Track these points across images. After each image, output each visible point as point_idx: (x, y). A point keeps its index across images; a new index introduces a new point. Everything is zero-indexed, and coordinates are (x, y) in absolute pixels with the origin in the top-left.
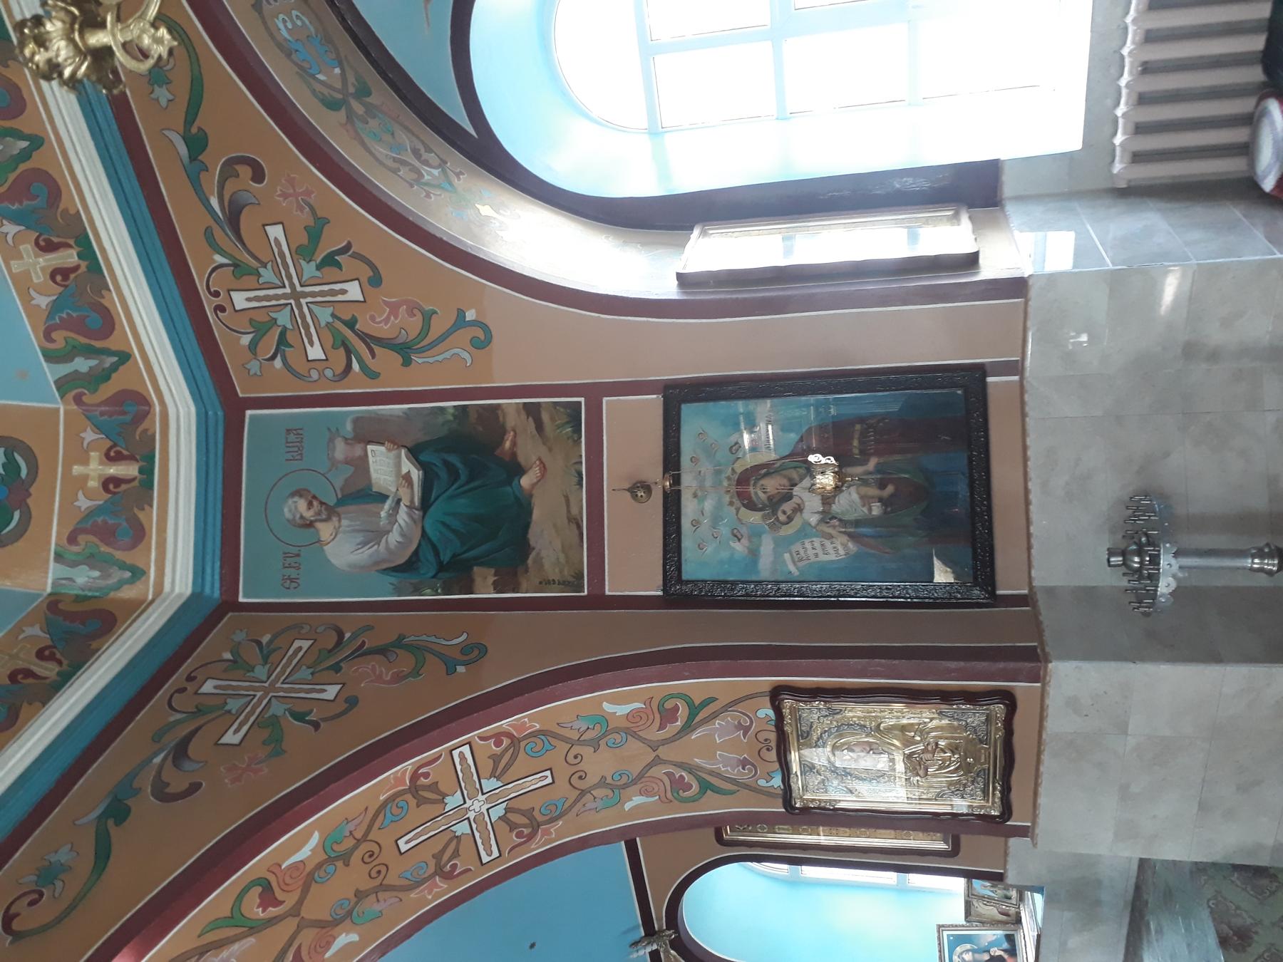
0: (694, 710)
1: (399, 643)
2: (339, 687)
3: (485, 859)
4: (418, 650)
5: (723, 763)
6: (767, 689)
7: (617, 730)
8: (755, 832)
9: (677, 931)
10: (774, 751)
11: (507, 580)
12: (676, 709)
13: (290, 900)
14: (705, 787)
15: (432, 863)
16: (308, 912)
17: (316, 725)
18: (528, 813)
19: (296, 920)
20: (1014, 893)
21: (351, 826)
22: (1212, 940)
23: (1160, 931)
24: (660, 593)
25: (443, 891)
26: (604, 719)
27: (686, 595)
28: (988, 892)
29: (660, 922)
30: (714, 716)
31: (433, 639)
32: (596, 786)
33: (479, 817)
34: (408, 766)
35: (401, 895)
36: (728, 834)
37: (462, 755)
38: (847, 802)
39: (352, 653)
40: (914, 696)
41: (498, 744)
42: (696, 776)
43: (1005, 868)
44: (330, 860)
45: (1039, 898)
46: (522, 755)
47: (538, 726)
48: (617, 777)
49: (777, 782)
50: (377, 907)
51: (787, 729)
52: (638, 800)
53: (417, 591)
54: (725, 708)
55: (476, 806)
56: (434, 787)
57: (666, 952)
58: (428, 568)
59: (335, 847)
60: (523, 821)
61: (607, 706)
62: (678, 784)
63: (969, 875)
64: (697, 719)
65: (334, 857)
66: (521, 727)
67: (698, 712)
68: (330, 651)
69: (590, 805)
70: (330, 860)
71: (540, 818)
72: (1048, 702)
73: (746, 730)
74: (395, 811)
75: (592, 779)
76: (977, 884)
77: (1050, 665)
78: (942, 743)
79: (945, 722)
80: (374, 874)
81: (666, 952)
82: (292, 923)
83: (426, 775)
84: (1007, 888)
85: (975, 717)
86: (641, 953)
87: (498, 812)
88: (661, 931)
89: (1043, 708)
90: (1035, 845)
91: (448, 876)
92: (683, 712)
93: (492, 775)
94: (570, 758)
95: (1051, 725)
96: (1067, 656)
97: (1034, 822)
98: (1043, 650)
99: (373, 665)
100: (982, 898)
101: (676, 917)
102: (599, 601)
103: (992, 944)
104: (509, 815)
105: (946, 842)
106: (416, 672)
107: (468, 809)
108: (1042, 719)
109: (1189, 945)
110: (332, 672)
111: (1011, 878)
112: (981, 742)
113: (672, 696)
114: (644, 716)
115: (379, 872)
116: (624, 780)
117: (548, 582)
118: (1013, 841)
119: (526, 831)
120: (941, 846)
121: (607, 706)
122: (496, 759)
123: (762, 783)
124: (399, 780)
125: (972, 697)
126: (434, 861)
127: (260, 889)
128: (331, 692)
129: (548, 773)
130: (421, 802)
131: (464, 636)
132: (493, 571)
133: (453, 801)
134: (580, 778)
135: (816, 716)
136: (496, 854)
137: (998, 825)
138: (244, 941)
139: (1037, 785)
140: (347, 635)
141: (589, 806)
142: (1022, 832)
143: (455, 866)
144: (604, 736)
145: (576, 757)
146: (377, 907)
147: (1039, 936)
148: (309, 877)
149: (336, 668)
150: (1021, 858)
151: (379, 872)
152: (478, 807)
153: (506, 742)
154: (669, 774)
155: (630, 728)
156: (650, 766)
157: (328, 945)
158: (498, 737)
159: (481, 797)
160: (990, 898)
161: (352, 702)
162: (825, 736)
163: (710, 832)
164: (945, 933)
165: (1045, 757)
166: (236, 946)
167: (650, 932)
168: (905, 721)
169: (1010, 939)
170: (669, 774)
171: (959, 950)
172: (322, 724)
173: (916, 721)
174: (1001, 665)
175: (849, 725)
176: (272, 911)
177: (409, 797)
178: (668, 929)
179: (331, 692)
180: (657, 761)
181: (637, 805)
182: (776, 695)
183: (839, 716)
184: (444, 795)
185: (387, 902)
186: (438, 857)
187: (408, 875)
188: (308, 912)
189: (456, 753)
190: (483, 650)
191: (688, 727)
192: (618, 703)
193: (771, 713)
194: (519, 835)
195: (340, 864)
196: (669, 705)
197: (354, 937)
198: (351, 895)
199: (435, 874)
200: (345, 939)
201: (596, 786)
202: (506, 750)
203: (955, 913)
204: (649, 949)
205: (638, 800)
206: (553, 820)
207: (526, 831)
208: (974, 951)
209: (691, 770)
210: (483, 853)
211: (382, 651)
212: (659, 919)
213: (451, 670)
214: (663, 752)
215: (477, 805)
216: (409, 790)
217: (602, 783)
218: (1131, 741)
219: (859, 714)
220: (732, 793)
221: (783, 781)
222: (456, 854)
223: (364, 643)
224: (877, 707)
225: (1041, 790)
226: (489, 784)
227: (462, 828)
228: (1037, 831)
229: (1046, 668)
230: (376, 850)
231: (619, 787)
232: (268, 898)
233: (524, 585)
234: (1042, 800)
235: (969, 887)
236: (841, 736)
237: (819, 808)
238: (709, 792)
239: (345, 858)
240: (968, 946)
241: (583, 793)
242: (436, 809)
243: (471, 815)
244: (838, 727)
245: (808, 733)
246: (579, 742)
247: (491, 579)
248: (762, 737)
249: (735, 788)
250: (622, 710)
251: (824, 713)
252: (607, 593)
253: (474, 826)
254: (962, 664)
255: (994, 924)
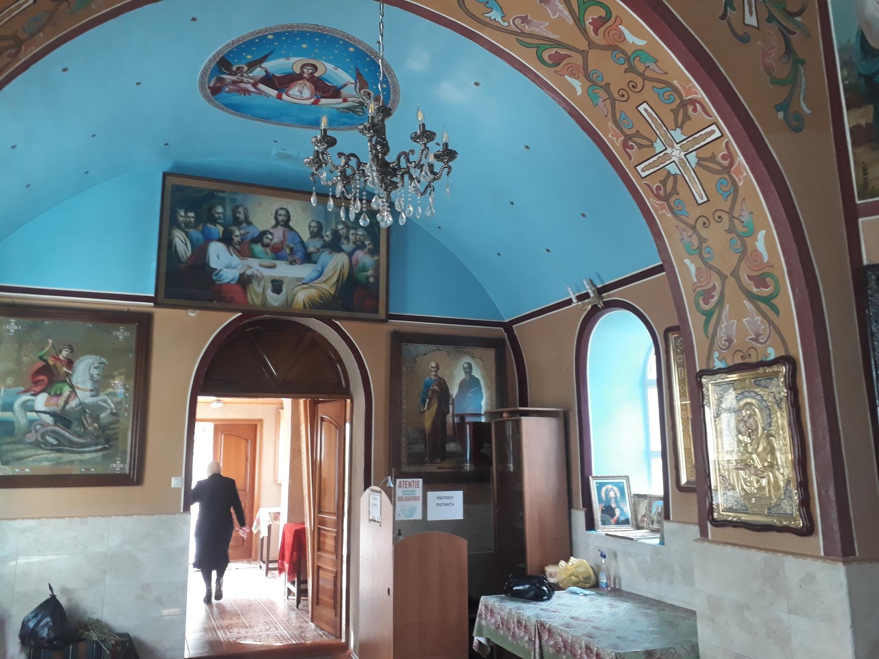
0: (767, 300)
1: (799, 61)
2: (756, 25)
3: (639, 168)
4: (793, 80)
5: (727, 326)
6: (792, 353)
7: (744, 245)
8: (676, 354)
9: (604, 308)
10: (741, 361)
11: (861, 135)
12: (767, 286)
13: (599, 39)
14: (708, 315)
15: (633, 131)
16: (593, 54)
17: (724, 16)
18: (675, 191)
19: (587, 48)
20: (656, 526)
21: (653, 66)
22: (649, 646)
23: (646, 615)
24: (865, 262)
25: (614, 143)
26: (753, 234)
27: (866, 283)
28: (654, 510)
29: (607, 296)
30: (765, 316)
31: (803, 87)
32: (700, 237)
33: (667, 156)
34: (701, 94)
35: (610, 116)
36: (672, 337)
37: (713, 132)
38: (709, 413)
39: (784, 27)
40: (801, 463)
41: (724, 157)
42: (715, 308)
43: (672, 521)
44: (628, 59)
45: (657, 541)
46: (718, 177)
47: (740, 184)
48: (708, 250)
49: (718, 365)
50: (600, 102)
51: (761, 370)
52: (692, 268)
53: (844, 64)
54: (771, 323)
55: (676, 153)
56: (687, 117)
57: (589, 303)
58: (865, 67)
59: (637, 59)
60: (669, 188)
61: (762, 234)
62: (707, 295)
63: (666, 498)
64: (760, 303)
65: (631, 61)
66: (739, 172)
67: (767, 304)
68: (784, 9)
69: (685, 235)
70: (628, 59)
71: (672, 200)
72: (809, 559)
73: (756, 340)
74: (667, 94)
75: (703, 232)
76: (661, 503)
77: (841, 564)
78: (764, 482)
79: (782, 484)
80: (621, 92)
81: (589, 303)
82: (583, 45)
83: (695, 110)
84: (659, 522)
85: (791, 506)
86: (587, 287)
87: (673, 169)
88: (602, 298)
89: (804, 556)
90: (696, 540)
91: (625, 145)
92: (765, 292)
93: (700, 159)
94: (718, 214)
95: (789, 561)
96: (848, 575)
97: (712, 542)
98: (852, 561)
99: (778, 47)
100: (650, 505)
101: (611, 307)
102: (852, 215)
103: (621, 510)
104: (672, 177)
105: (688, 482)
106: (775, 81)
107: (673, 147)
108: (795, 554)
109: (641, 631)
110: (767, 16)
111: (666, 525)
112: (769, 509)
113: (776, 282)
114: (756, 264)
115: (623, 96)
116: (705, 255)
117: (865, 171)
118: (696, 529)
119: (661, 192)
120: (684, 480)
121: (762, 234)
122: (713, 158)
123: (716, 354)
124: (689, 91)
125: (805, 503)
126: (634, 132)
127: (604, 15)
128: (751, 20)
129: (705, 199)
130: (675, 112)
131: (807, 111)
132: (871, 121)
133: (678, 135)
134: (704, 223)
135: (774, 390)
136: (643, 174)
137: (707, 517)
138: (570, 17)
139: (740, 546)
140: (799, 19)
141: (685, 235)
142: (704, 533)
143: (632, 148)
144: (739, 236)
145: (720, 217)
146: (600, 102)
147: (632, 539)
148: (615, 47)
149: (771, 19)
150: (684, 533)
151: (623, 96)
152: (676, 154)
153: (726, 163)
154: (714, 287)
155: (745, 252)
156: (719, 273)
157: (573, 75)
158: (730, 156)
159: (683, 154)
160: (651, 511)
161: (745, 39)
162: (759, 398)
163: (675, 322)
164: (624, 481)
165: (762, 555)
166: (566, 13)
167: (600, 291)
168: (778, 455)
169: (626, 522)
170: (714, 287)
171: (615, 489)
172: (725, 21)
173: (780, 463)
174: (836, 527)
175: (770, 415)
176: (590, 29)
177: (678, 101)
178: (604, 302)
179: (751, 20)
180: (723, 278)
181: (688, 268)
182: (789, 360)
183: (776, 407)
184: (681, 127)
185: (604, 107)
186: (638, 134)
187: (623, 116)
188: (593, 54)
189: (714, 127)
190: (797, 130)
191: (752, 297)
192: (767, 242)
193: (772, 357)
194: (658, 188)
195: (626, 66)
196: (769, 280)
197: (579, 91)
198: (606, 81)
199: (626, 136)
200: (577, 85)
201: (700, 237)
202: (720, 164)
203: (638, 488)
204: (590, 291)
205: (692, 268)
206: (671, 209)
207: (661, 192)
208: (616, 498)
209: (720, 303)
210: (643, 165)
211: (789, 49)
212: (609, 296)
213: (779, 108)
214: (731, 280)
215: (676, 153)
216: (682, 100)
217: (702, 240)
218: (784, 616)
219: (780, 422)
220: (707, 336)
221: (720, 369)
222: (641, 146)
223: (794, 33)
224: (787, 435)
225: (737, 549)
226: (693, 158)
227: (659, 146)
228: (706, 543)
229: (839, 561)
230: (638, 90)
231: (699, 253)
232: (598, 23)
233: (859, 151)
234: (729, 548)
235: (659, 498)
236: (761, 410)
237: (703, 395)
238: (704, 318)
239: (631, 69)
240: (618, 495)
241: (693, 228)
242: (670, 121)
243: (669, 151)
244: (767, 407)
245: (759, 385)
246: (732, 218)
247: (863, 122)
248: (752, 351)
249: (710, 335)
250: (760, 245)
251: (777, 396)
252: (860, 220)
253: (661, 155)
254: (833, 498)
255: (635, 512)
